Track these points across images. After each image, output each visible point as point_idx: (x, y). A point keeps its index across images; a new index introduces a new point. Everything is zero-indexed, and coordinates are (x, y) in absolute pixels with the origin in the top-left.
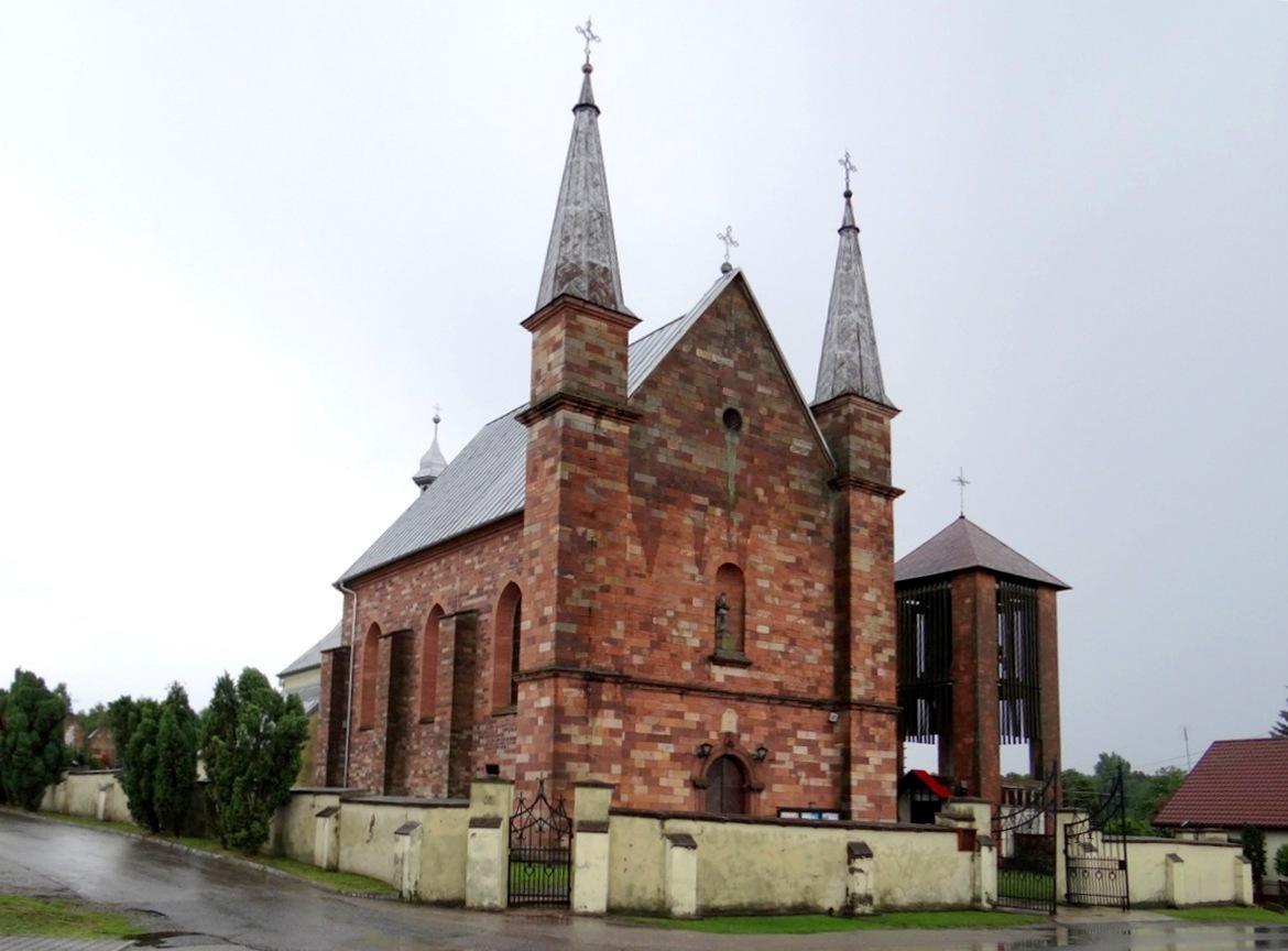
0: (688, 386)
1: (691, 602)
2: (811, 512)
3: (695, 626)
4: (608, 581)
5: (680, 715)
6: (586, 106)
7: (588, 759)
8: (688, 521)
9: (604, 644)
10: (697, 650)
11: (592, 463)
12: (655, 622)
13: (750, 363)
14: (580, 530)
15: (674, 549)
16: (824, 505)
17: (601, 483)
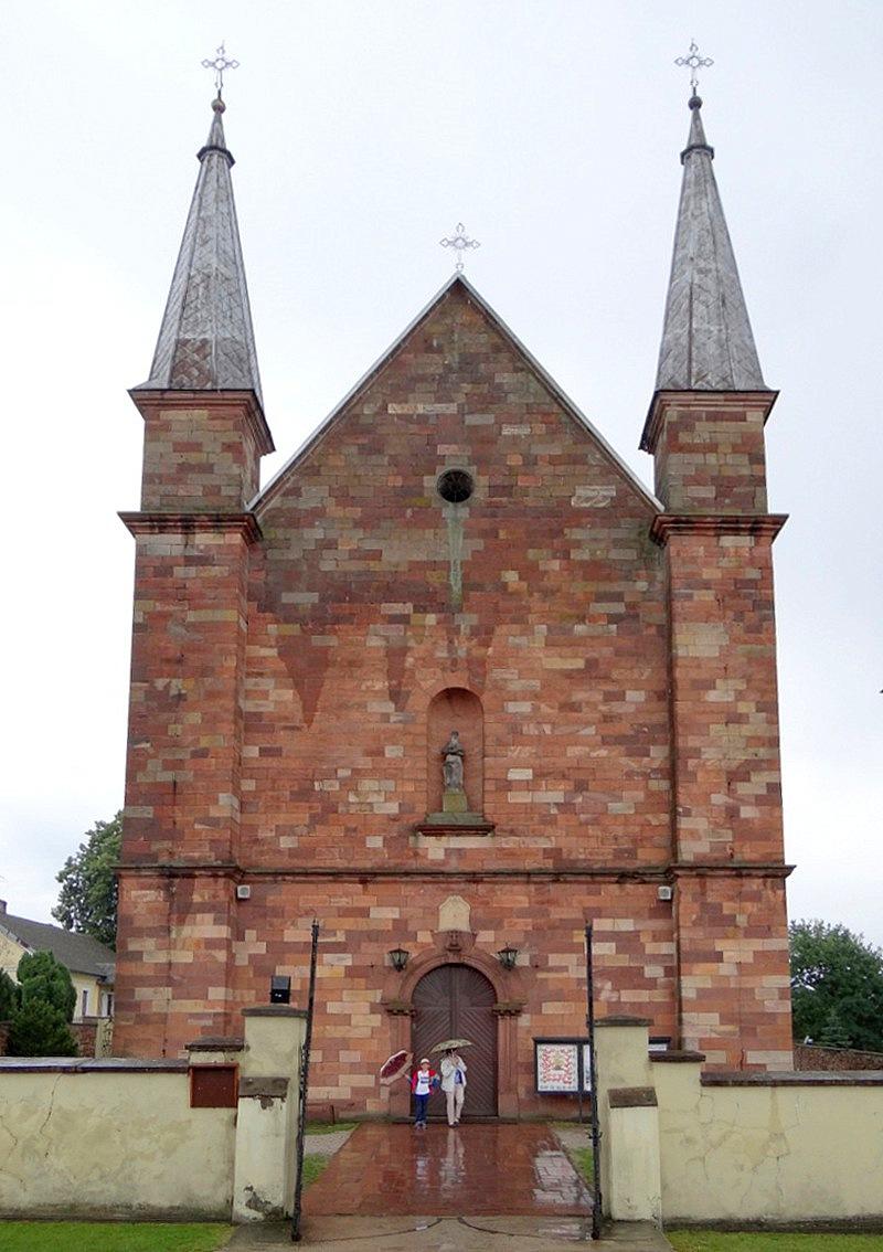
0: (374, 459)
1: (381, 753)
2: (616, 587)
3: (390, 785)
4: (204, 743)
5: (364, 913)
6: (216, 152)
7: (170, 982)
8: (375, 641)
9: (197, 826)
10: (394, 819)
11: (183, 595)
12: (317, 788)
13: (491, 399)
14: (160, 683)
15: (349, 685)
16: (643, 572)
17: (192, 617)
